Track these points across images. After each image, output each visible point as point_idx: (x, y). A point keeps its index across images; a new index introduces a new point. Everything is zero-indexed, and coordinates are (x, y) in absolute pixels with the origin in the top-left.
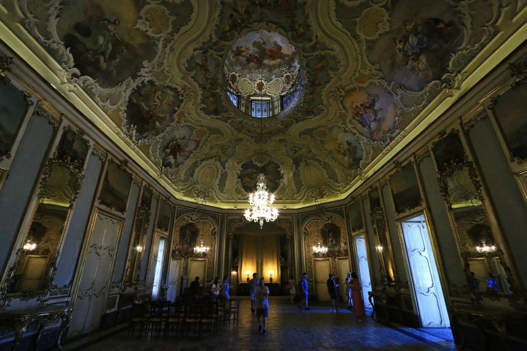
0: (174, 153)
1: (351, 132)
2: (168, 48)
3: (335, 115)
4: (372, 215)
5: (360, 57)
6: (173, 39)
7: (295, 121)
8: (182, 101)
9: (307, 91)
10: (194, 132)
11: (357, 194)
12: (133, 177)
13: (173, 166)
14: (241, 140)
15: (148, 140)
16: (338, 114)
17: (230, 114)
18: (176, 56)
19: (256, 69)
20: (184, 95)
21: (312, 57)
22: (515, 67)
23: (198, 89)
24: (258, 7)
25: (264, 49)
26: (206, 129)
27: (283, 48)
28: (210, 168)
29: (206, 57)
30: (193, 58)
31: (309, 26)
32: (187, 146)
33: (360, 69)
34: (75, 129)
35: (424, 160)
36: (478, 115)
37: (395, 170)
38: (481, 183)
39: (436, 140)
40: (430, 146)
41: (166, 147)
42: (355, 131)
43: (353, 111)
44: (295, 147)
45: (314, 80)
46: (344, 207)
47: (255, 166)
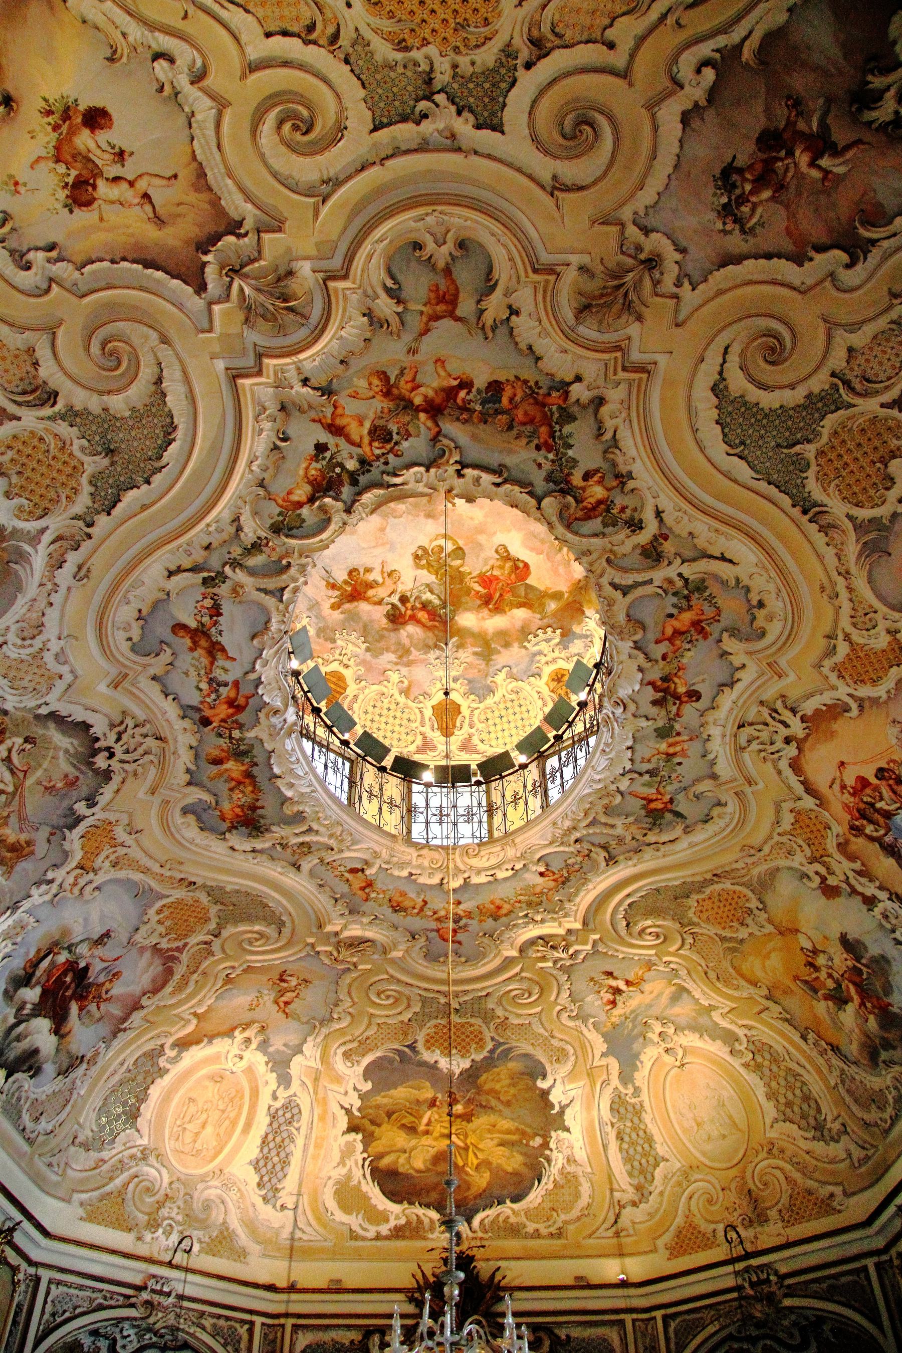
0: (54, 1007)
1: (854, 891)
2: (69, 567)
5: (841, 582)
6: (89, 536)
7: (600, 856)
8: (106, 775)
9: (643, 723)
10: (152, 912)
13: (49, 1069)
14: (357, 944)
16: (788, 819)
17: (310, 830)
18: (97, 599)
19: (427, 648)
20: (118, 749)
21: (649, 590)
24: (422, 416)
25: (459, 577)
26: (204, 899)
27: (532, 568)
31: (622, 478)
32: (117, 975)
33: (849, 629)
41: (24, 980)
42: (870, 890)
43: (847, 798)
44: (610, 974)
45: (666, 679)
46: (870, 1263)
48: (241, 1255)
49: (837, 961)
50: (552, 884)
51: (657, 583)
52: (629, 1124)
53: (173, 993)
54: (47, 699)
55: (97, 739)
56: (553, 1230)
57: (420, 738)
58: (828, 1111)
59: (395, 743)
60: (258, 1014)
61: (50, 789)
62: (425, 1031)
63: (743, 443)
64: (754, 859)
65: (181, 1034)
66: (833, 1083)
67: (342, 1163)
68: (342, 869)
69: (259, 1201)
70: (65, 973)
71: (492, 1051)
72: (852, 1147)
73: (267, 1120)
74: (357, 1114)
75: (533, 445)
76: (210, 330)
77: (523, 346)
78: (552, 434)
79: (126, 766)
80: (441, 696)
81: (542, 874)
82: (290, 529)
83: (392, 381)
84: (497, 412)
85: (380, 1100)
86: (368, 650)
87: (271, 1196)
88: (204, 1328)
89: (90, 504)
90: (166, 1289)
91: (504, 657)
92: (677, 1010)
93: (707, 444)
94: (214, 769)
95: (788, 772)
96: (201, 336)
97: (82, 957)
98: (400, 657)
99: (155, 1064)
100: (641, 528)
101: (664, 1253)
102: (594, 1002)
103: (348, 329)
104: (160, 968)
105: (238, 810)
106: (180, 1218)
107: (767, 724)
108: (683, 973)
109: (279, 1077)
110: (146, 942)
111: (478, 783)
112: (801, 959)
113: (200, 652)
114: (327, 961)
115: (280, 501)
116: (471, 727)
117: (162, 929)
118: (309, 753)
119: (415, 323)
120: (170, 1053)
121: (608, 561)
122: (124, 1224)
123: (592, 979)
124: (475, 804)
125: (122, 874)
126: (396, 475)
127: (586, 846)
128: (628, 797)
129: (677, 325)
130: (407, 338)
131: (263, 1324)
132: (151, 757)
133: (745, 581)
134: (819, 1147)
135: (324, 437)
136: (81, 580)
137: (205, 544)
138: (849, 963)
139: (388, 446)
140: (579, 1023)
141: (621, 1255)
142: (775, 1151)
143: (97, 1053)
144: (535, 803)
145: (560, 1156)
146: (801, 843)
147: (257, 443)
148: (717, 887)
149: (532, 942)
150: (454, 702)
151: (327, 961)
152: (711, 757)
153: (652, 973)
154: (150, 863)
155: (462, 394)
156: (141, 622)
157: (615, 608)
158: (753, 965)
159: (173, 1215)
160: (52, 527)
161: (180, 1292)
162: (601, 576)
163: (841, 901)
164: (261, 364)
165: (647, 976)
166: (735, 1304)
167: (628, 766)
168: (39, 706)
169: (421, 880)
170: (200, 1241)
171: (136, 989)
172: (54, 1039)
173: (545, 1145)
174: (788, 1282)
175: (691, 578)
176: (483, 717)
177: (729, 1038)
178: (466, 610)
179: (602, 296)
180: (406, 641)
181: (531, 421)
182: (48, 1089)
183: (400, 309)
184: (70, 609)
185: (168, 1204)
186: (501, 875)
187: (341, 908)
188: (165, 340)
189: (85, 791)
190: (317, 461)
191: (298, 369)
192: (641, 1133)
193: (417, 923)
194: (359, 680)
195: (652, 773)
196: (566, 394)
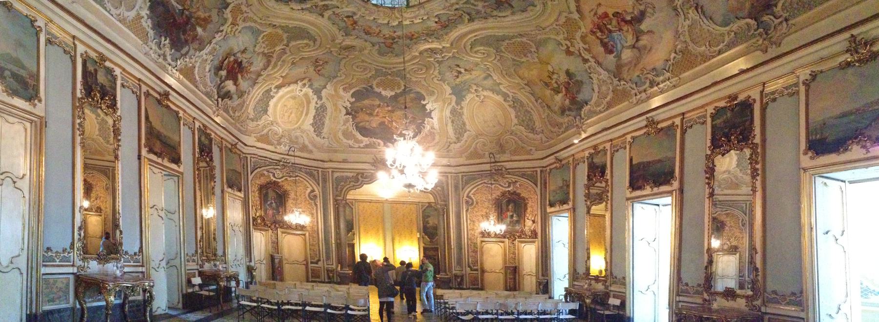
3: (557, 20)
4: (588, 187)
10: (260, 38)
11: (567, 155)
12: (181, 115)
13: (235, 97)
15: (191, 58)
16: (563, 20)
22: (855, 42)
26: (280, 31)
28: (294, 98)
34: (93, 55)
35: (695, 127)
36: (786, 88)
37: (645, 130)
38: (759, 172)
39: (722, 104)
40: (710, 110)
41: (220, 68)
42: (587, 57)
44: (458, 66)
47: (379, 95)
48: (311, 152)
58: (538, 125)
60: (307, 75)
67: (344, 124)
69: (315, 136)
85: (358, 104)
87: (319, 134)
92: (485, 82)
108: (491, 69)
117: (264, 45)
127: (461, 12)
134: (531, 135)
149: (426, 50)
158: (525, 73)
163: (572, 57)
169: (379, 21)
171: (259, 68)
177: (505, 96)
182: (236, 103)
193: (375, 40)
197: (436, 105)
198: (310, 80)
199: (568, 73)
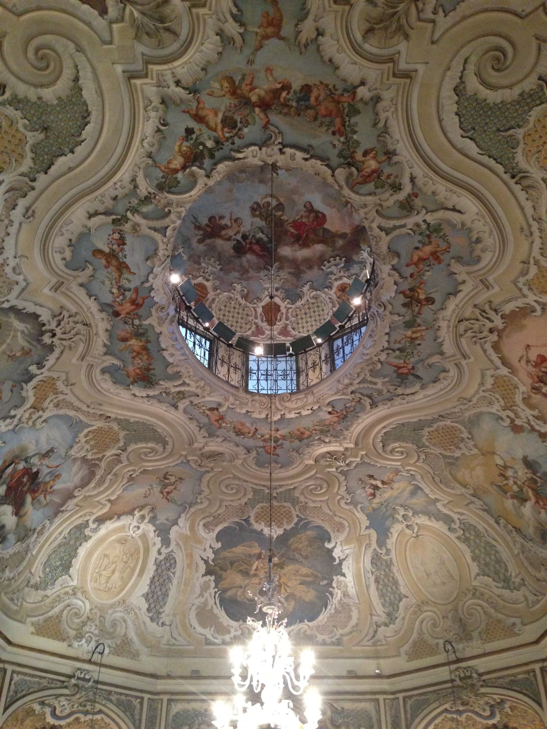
1: (533, 429)
2: (20, 209)
3: (482, 384)
5: (535, 226)
6: (33, 189)
8: (51, 348)
9: (396, 318)
10: (81, 435)
13: (12, 538)
14: (214, 456)
17: (184, 384)
19: (259, 269)
20: (58, 331)
21: (404, 231)
23: (99, 316)
24: (257, 110)
25: (280, 223)
26: (116, 427)
27: (328, 218)
28: (123, 541)
29: (120, 232)
30: (85, 235)
31: (390, 154)
32: (58, 476)
33: (539, 257)
43: (530, 368)
44: (371, 477)
45: (412, 290)
46: (537, 667)
48: (135, 655)
49: (520, 474)
50: (336, 419)
51: (410, 227)
52: (383, 573)
53: (94, 488)
54: (8, 297)
55: (44, 325)
56: (334, 639)
57: (254, 326)
58: (513, 569)
59: (238, 329)
61: (12, 357)
62: (255, 510)
63: (474, 129)
64: (466, 407)
65: (100, 513)
66: (516, 552)
67: (201, 595)
68: (204, 408)
70: (23, 476)
71: (297, 524)
72: (528, 594)
73: (154, 568)
74: (211, 563)
75: (330, 131)
76: (111, 43)
77: (326, 59)
78: (344, 125)
79: (64, 342)
80: (268, 299)
81: (330, 413)
82: (170, 188)
83: (237, 83)
84: (308, 108)
85: (227, 554)
86: (221, 269)
88: (111, 701)
89: (33, 166)
90: (87, 677)
91: (309, 275)
92: (414, 500)
93: (448, 129)
94: (122, 345)
95: (491, 351)
96: (105, 47)
97: (34, 465)
98: (242, 275)
99: (82, 533)
100: (400, 189)
101: (405, 657)
102: (362, 494)
103: (206, 44)
104: (86, 472)
105: (138, 371)
106: (97, 632)
107: (478, 320)
108: (418, 477)
109: (162, 541)
110: (78, 455)
111: (291, 355)
112: (496, 472)
113: (112, 269)
114: (194, 466)
115: (163, 168)
116: (287, 320)
117: (88, 447)
118: (184, 334)
119: (252, 41)
120: (92, 526)
121: (377, 211)
122: (60, 636)
123: (360, 480)
124: (289, 368)
125: (62, 412)
126: (241, 152)
128: (386, 365)
129: (433, 43)
130: (247, 51)
131: (149, 699)
132: (81, 337)
133: (469, 224)
134: (506, 593)
135: (192, 124)
136: (29, 218)
137: (113, 196)
138: (528, 475)
139: (235, 131)
140: (351, 507)
141: (377, 658)
142: (477, 594)
143: (44, 527)
144: (325, 368)
145: (339, 592)
146: (498, 396)
147: (147, 127)
148: (441, 424)
149: (323, 456)
150: (276, 304)
151: (194, 466)
152: (440, 340)
153: (398, 477)
154: (80, 405)
155: (284, 94)
156: (72, 248)
157: (381, 243)
159: (92, 630)
160: (6, 181)
161: (96, 678)
162: (372, 221)
164: (147, 68)
165: (396, 478)
166: (450, 690)
167: (386, 345)
168: (3, 302)
170: (109, 647)
171: (70, 485)
172: (14, 519)
173: (330, 585)
174: (485, 677)
175: (432, 223)
176: (294, 314)
177: (448, 520)
178: (285, 245)
179: (382, 21)
180: (246, 265)
181: (329, 114)
182: (11, 551)
183: (242, 30)
184: (23, 236)
185: (89, 623)
186: (304, 413)
187: (204, 432)
188: (80, 49)
189: (36, 358)
190: (187, 141)
191: (173, 73)
192: (391, 579)
193: (250, 442)
194: (215, 289)
195: (401, 350)
196: (355, 93)
197: (348, 549)
198: (153, 510)
199: (529, 464)
